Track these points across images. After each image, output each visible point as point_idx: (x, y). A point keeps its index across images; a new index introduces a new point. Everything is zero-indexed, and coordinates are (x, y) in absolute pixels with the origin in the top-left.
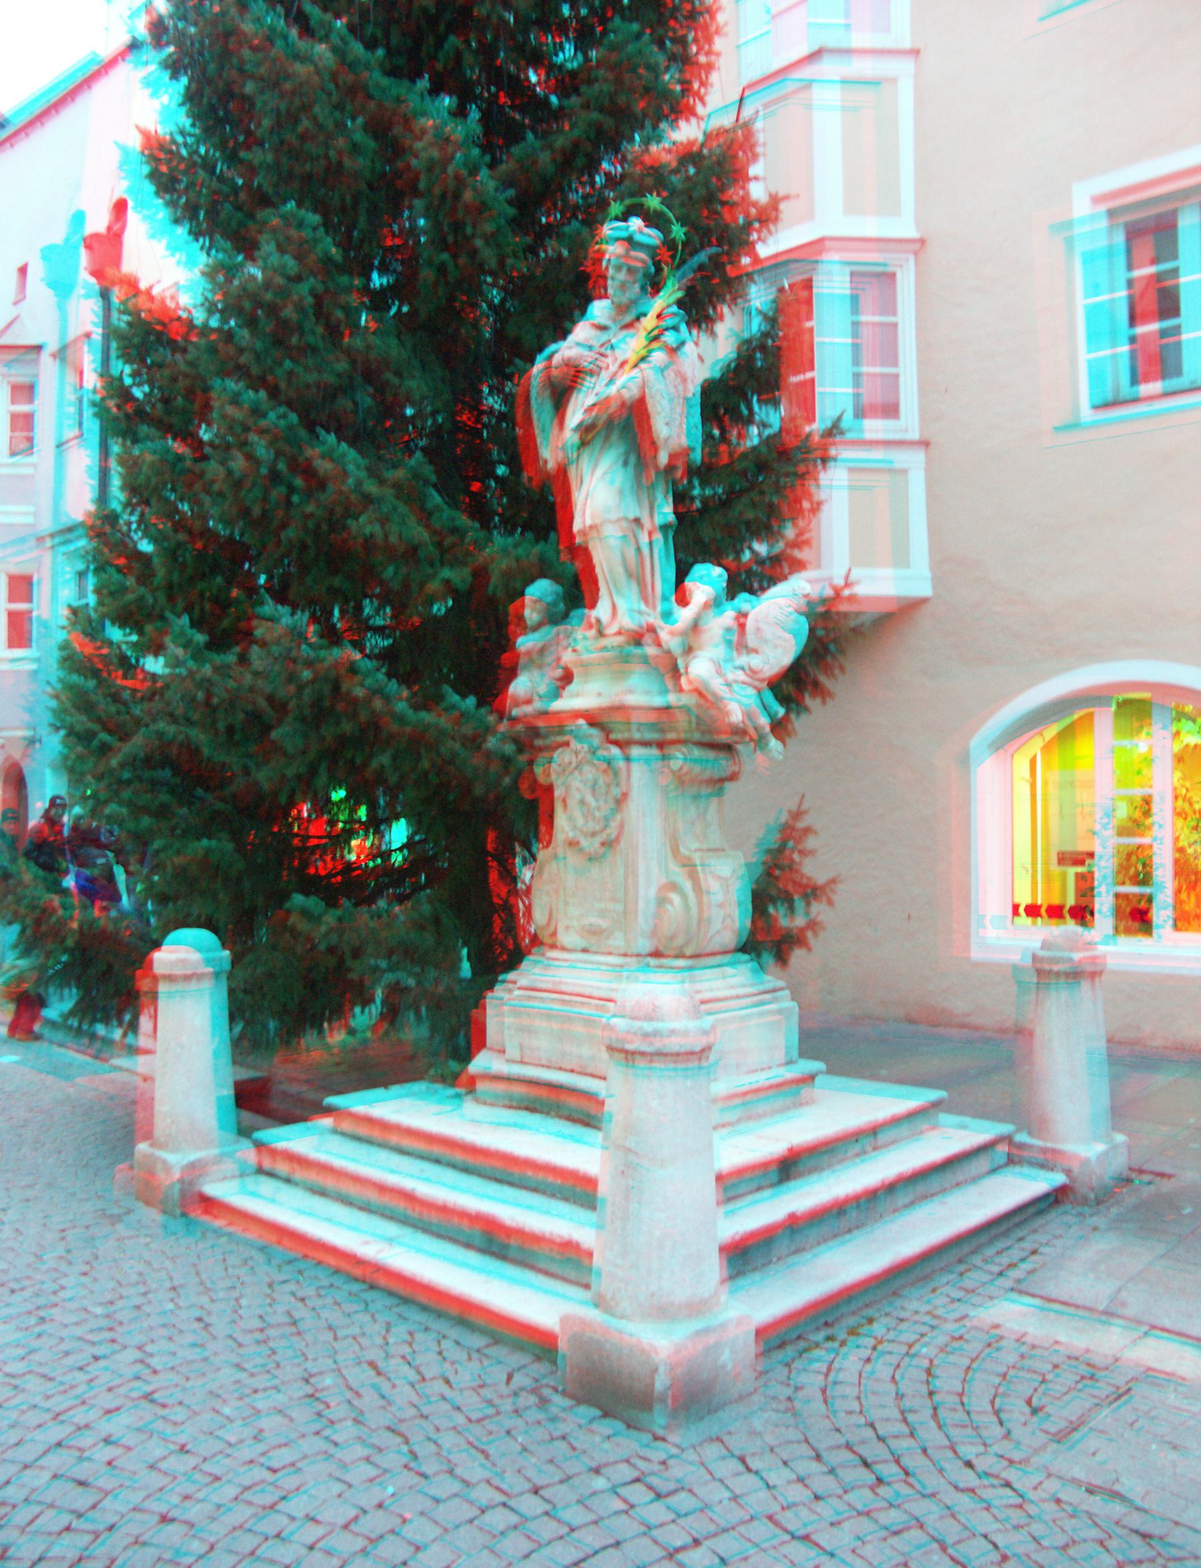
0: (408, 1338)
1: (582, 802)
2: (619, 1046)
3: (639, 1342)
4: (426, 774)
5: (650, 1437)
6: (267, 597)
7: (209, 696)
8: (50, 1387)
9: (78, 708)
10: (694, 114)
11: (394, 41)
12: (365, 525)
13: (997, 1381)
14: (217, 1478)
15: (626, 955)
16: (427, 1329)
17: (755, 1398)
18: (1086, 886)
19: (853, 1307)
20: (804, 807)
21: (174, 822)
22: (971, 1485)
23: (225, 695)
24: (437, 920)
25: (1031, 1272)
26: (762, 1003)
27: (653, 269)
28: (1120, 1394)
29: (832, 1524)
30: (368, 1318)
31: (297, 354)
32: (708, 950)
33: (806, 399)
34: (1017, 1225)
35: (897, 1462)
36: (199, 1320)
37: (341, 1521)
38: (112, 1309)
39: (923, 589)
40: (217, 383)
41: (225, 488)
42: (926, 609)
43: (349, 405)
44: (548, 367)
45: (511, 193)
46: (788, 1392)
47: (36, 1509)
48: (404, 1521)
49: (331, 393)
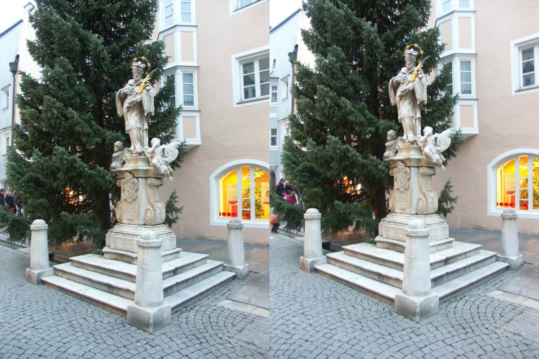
1: (400, 180)
20: (450, 181)
32: (428, 213)
39: (199, 143)
49: (344, 88)
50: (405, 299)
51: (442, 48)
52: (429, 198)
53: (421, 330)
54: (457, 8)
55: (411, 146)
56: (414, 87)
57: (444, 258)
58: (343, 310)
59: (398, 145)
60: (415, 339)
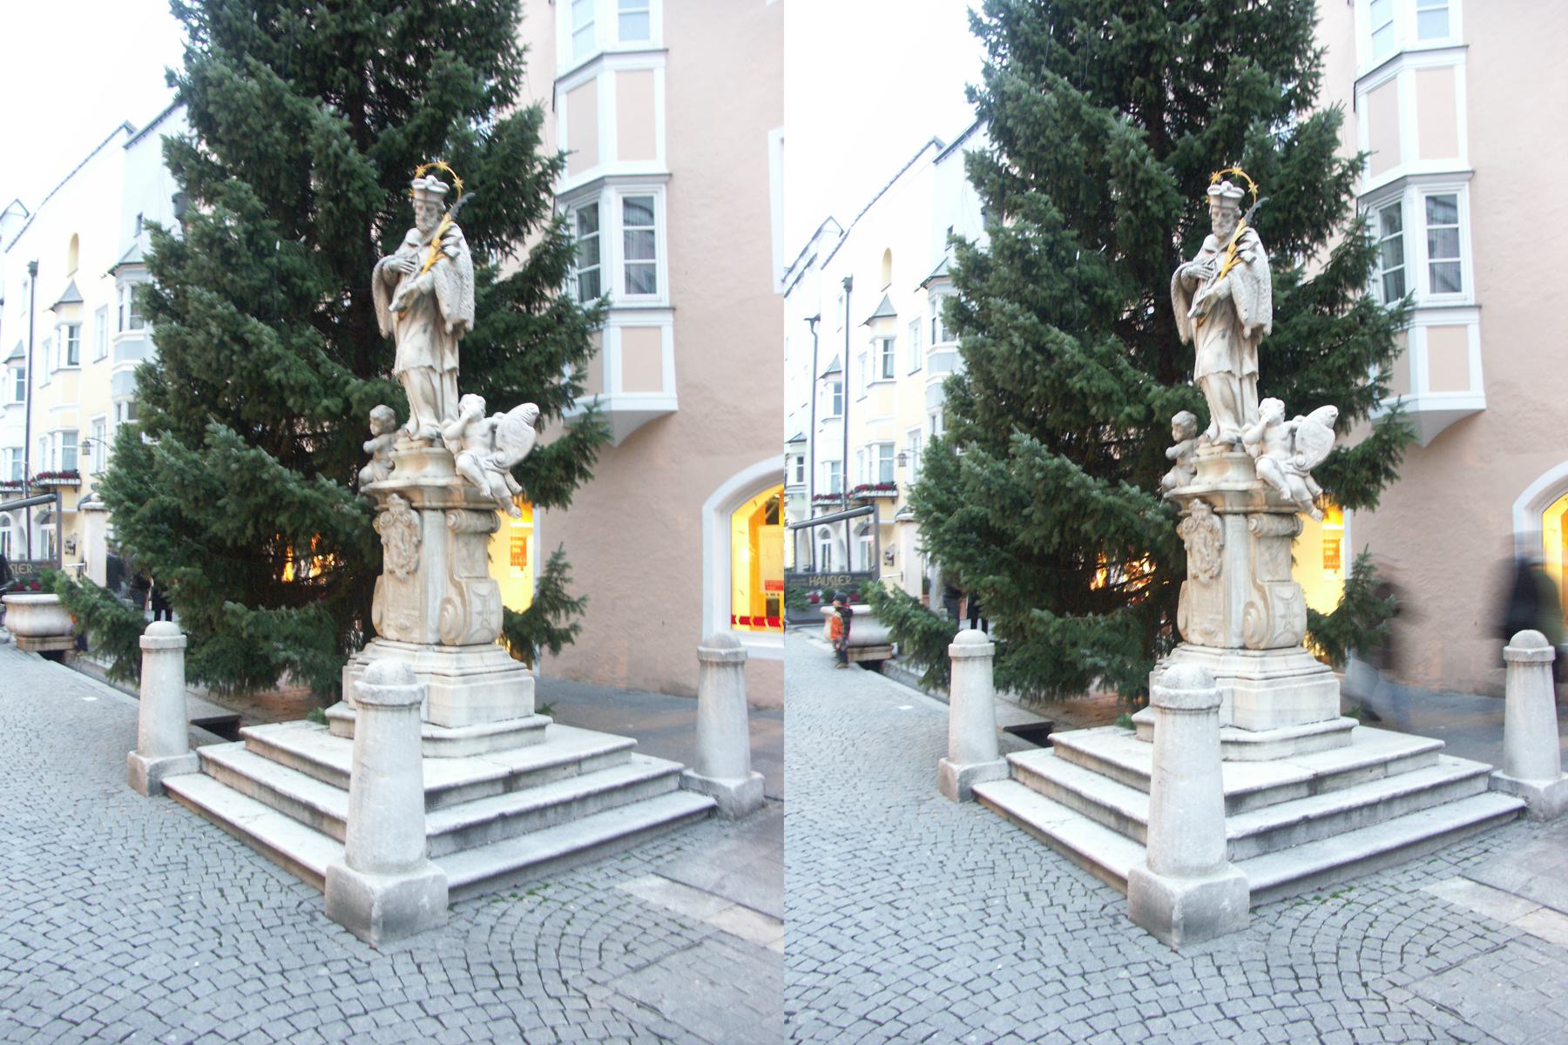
1: (396, 546)
7: (989, 489)
8: (842, 893)
12: (274, 374)
17: (446, 929)
19: (538, 876)
20: (563, 549)
23: (192, 478)
26: (507, 677)
28: (694, 945)
32: (471, 642)
34: (1482, 833)
42: (674, 419)
49: (259, 291)
50: (348, 878)
51: (555, 165)
52: (473, 598)
53: (373, 969)
54: (612, 43)
55: (1227, 454)
56: (433, 284)
57: (1306, 774)
58: (191, 898)
59: (396, 446)
60: (346, 988)
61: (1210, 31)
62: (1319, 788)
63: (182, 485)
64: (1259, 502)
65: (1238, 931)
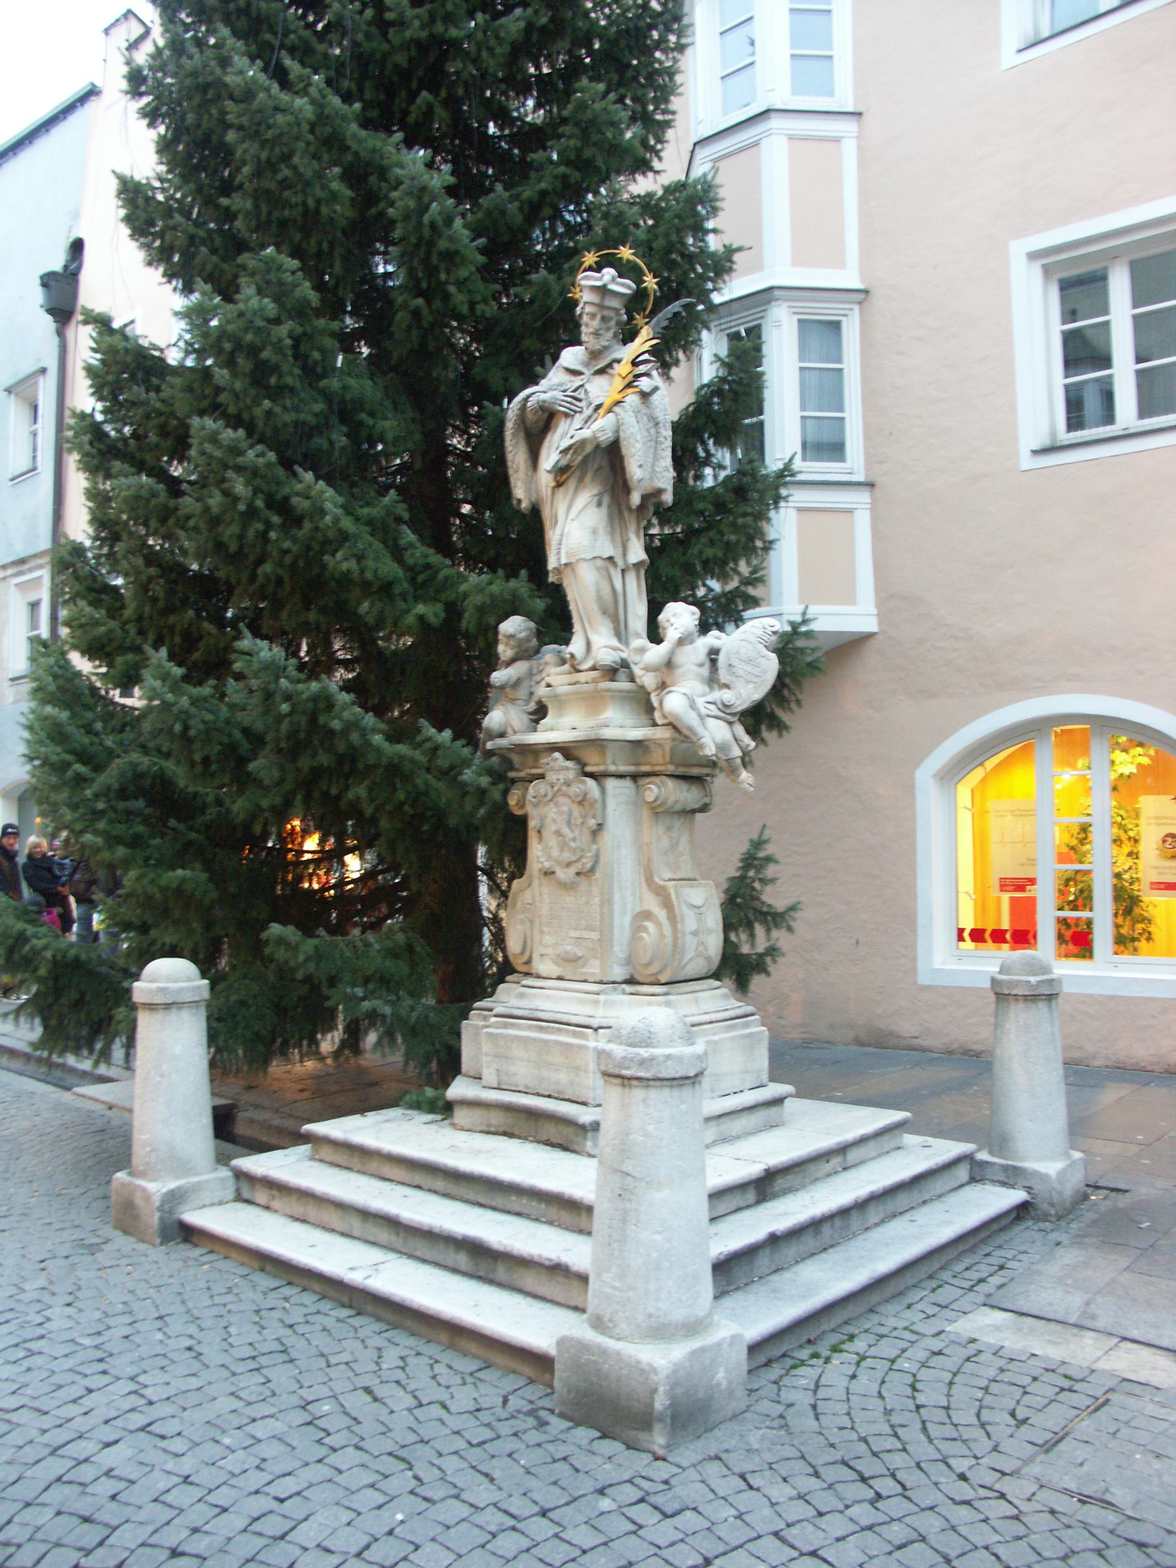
0: (401, 1364)
1: (558, 833)
2: (616, 1071)
3: (639, 1362)
4: (402, 804)
5: (650, 1457)
6: (245, 630)
7: (186, 728)
8: (47, 1422)
9: (52, 739)
10: (651, 169)
11: (368, 95)
12: (340, 562)
13: (980, 1394)
14: (225, 1510)
15: (601, 982)
16: (418, 1354)
18: (1024, 910)
21: (149, 852)
22: (968, 1498)
23: (201, 727)
24: (410, 948)
25: (1000, 1287)
27: (625, 317)
29: (838, 1539)
30: (358, 1344)
31: (276, 394)
33: (756, 440)
34: (983, 1241)
35: (893, 1476)
36: (190, 1349)
37: (354, 1550)
38: (99, 1340)
39: (869, 625)
40: (196, 421)
41: (203, 525)
42: (872, 644)
43: (325, 446)
44: (523, 408)
45: (482, 241)
46: (779, 1409)
47: (43, 1548)
48: (417, 1547)
50: (604, 1352)
56: (617, 431)
57: (754, 1170)
58: (326, 1408)
61: (535, 38)
62: (769, 1191)
63: (185, 737)
64: (658, 759)
65: (734, 1416)
